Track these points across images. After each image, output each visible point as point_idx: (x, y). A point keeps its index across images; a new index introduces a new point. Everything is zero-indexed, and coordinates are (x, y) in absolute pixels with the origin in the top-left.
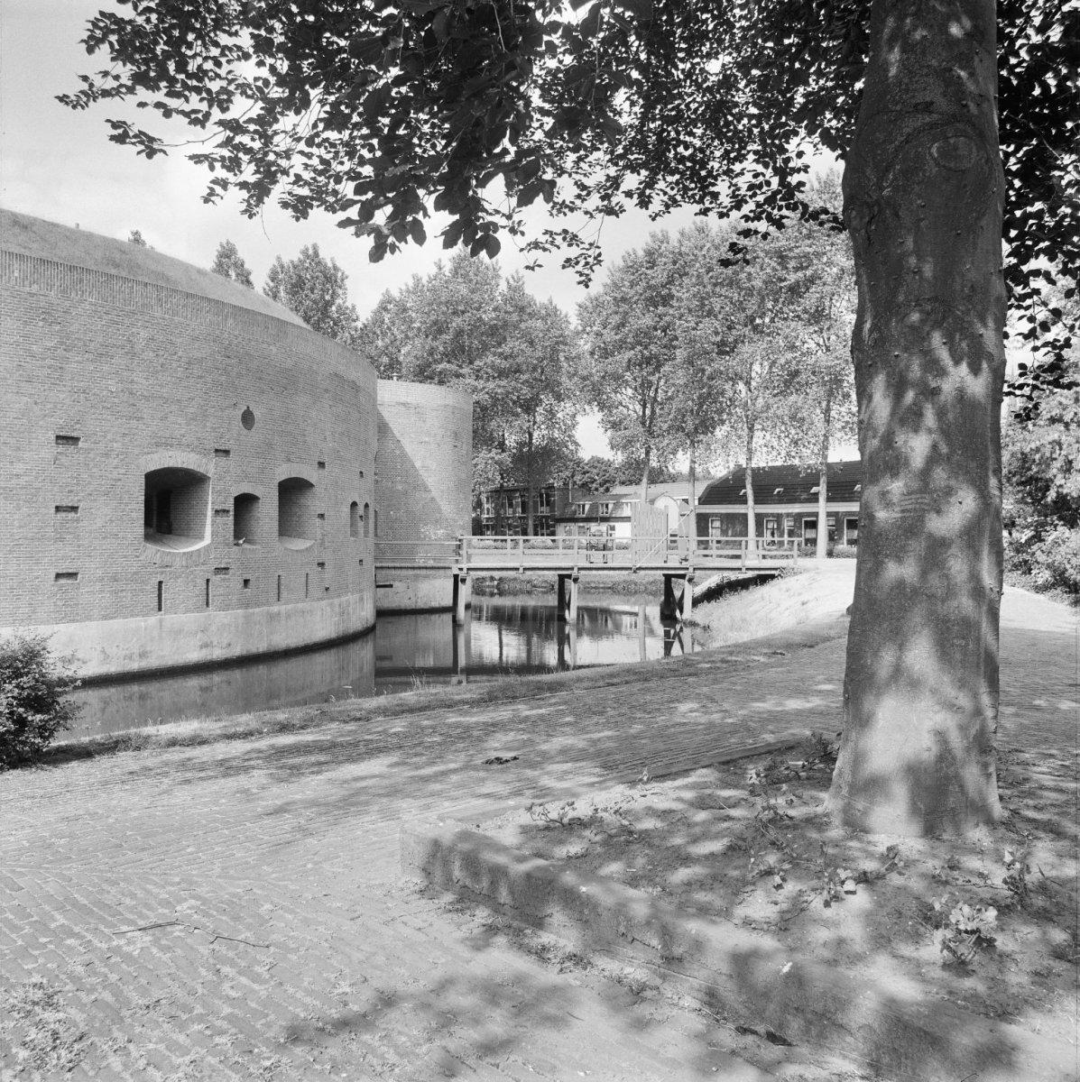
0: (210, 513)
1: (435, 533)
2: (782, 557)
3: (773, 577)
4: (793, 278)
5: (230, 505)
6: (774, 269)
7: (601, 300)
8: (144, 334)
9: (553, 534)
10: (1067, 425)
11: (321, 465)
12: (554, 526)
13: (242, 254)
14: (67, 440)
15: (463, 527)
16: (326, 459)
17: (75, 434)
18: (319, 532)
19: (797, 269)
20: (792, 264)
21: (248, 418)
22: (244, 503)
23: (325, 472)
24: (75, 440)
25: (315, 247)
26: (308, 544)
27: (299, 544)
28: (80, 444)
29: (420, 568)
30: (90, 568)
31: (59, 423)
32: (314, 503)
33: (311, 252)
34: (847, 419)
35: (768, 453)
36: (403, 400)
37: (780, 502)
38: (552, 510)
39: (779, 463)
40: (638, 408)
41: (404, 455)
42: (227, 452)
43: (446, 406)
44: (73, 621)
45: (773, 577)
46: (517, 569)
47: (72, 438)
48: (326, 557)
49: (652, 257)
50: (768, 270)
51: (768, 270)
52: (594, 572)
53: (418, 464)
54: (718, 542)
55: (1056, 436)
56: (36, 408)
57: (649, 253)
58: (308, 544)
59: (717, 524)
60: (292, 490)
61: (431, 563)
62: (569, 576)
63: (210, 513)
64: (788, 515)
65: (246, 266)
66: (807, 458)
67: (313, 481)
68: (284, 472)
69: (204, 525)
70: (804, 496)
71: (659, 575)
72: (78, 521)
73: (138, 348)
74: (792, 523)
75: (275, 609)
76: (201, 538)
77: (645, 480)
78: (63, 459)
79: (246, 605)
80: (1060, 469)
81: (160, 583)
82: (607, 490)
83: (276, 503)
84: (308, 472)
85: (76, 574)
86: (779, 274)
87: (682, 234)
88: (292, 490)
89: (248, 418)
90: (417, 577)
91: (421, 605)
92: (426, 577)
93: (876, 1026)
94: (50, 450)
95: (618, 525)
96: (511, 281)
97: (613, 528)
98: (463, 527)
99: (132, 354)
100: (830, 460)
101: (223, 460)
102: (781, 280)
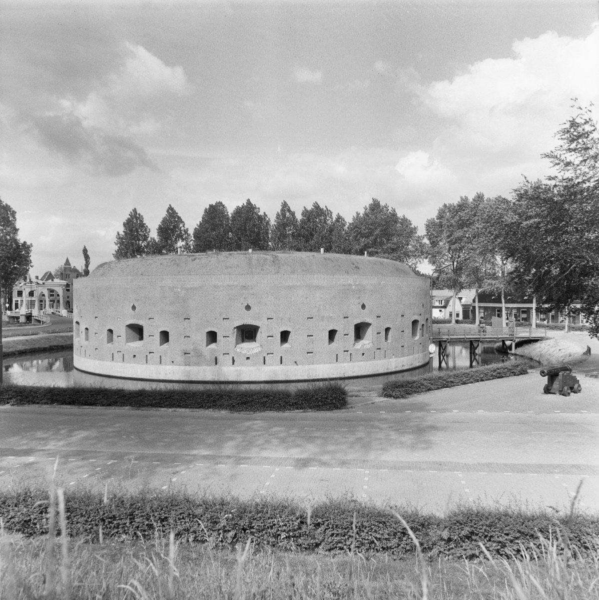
3: (539, 340)
30: (406, 346)
45: (539, 340)
63: (419, 329)
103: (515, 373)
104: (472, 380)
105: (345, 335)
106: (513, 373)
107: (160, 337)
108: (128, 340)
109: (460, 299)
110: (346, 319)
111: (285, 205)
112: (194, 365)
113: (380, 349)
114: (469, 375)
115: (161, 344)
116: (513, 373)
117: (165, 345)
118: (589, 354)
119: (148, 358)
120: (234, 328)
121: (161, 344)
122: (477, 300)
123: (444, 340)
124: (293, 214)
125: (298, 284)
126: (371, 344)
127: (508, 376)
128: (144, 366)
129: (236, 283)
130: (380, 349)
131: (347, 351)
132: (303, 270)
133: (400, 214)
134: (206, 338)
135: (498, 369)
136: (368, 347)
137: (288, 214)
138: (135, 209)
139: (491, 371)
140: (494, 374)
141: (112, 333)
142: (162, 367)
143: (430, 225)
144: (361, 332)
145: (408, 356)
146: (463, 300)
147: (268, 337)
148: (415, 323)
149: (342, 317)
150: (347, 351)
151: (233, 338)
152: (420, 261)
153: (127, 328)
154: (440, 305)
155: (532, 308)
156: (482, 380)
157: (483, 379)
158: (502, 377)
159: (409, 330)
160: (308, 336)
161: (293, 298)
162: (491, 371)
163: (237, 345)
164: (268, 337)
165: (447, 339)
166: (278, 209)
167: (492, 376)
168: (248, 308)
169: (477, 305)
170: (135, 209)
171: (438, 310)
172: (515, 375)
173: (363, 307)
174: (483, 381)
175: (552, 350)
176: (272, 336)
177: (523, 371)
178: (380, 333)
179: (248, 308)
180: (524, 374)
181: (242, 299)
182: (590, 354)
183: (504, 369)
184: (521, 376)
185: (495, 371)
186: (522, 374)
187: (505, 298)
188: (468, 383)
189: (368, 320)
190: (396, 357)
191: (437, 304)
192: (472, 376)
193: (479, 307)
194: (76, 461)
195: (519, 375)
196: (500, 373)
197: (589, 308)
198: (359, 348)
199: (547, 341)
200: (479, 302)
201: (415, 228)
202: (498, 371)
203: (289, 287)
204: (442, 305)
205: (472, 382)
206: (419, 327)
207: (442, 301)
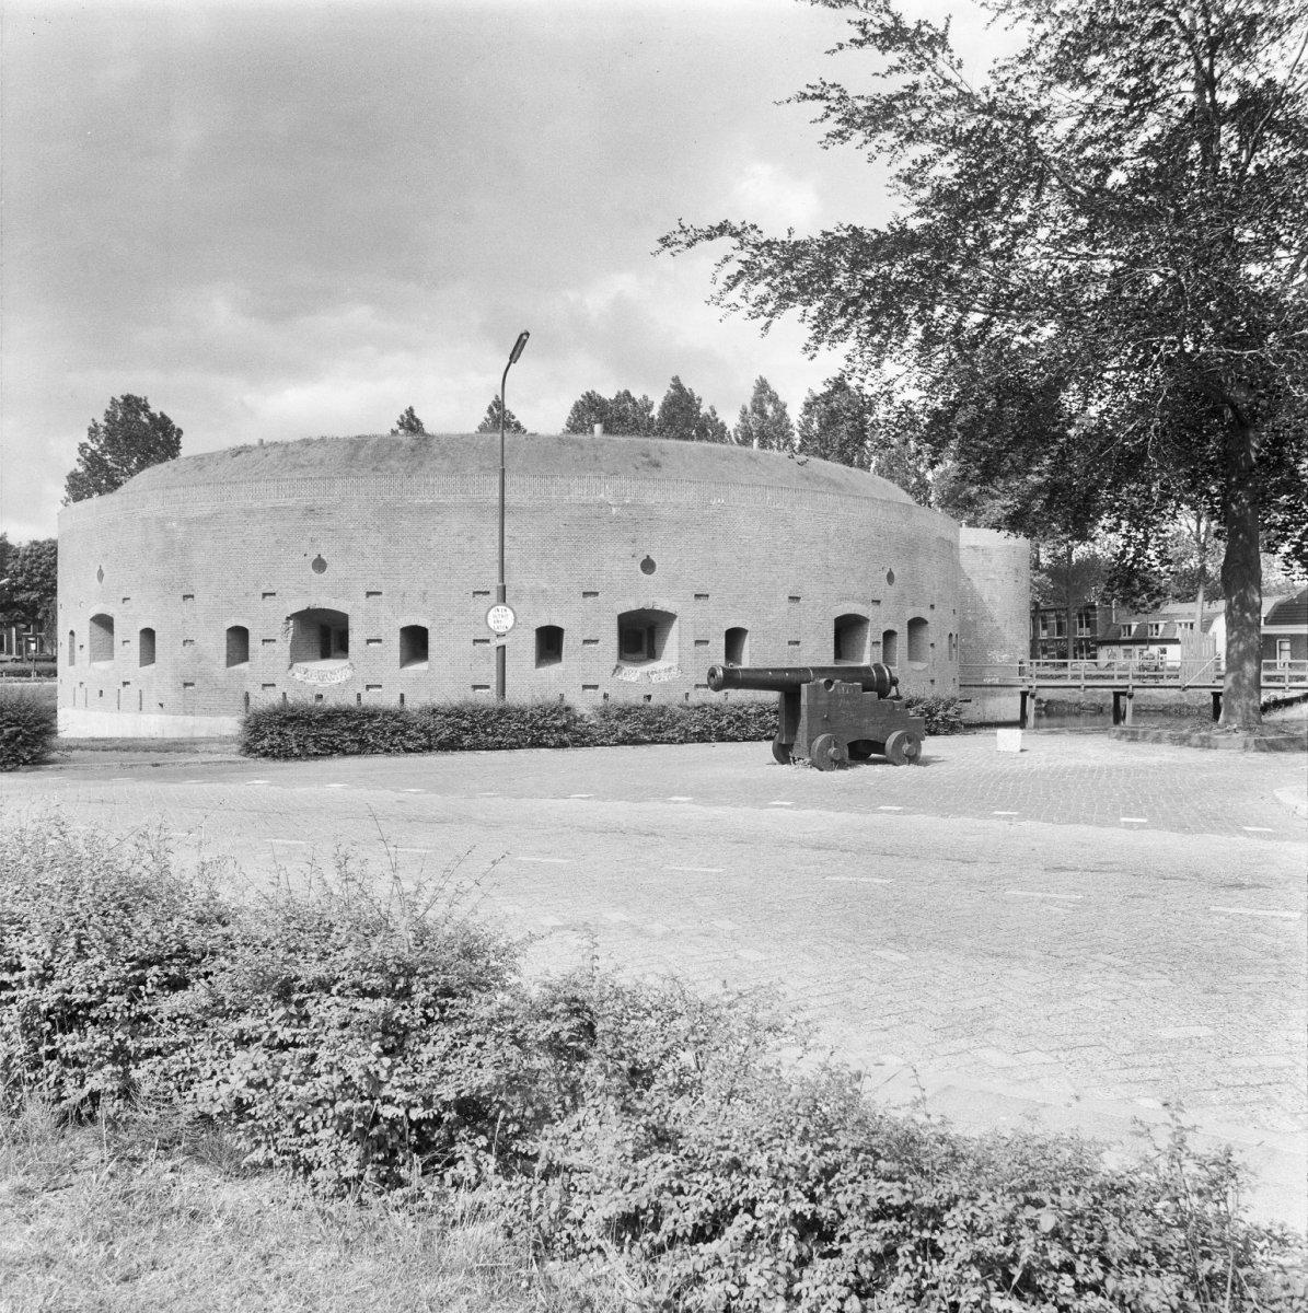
1: (999, 657)
5: (881, 639)
8: (833, 527)
9: (1094, 657)
11: (932, 607)
12: (1095, 649)
13: (775, 386)
15: (1023, 652)
16: (935, 602)
18: (931, 656)
21: (890, 577)
23: (934, 612)
24: (798, 599)
26: (925, 665)
27: (919, 666)
29: (986, 686)
31: (790, 589)
32: (929, 635)
36: (972, 543)
38: (1093, 631)
41: (973, 590)
42: (878, 602)
48: (935, 676)
53: (985, 598)
54: (1290, 664)
58: (925, 665)
59: (1287, 646)
60: (916, 624)
61: (997, 682)
62: (1124, 694)
63: (868, 642)
65: (780, 399)
67: (927, 619)
68: (910, 614)
71: (1207, 692)
73: (831, 537)
77: (1200, 597)
82: (1157, 606)
84: (926, 614)
88: (916, 624)
89: (890, 577)
90: (985, 694)
91: (988, 719)
92: (993, 695)
94: (786, 605)
95: (1169, 647)
97: (1164, 651)
98: (1023, 652)
101: (876, 608)
105: (585, 642)
107: (228, 641)
108: (297, 656)
110: (590, 599)
111: (763, 386)
112: (201, 714)
115: (405, 662)
117: (419, 667)
119: (122, 697)
120: (288, 618)
121: (405, 662)
124: (781, 410)
125: (450, 499)
126: (675, 673)
128: (115, 715)
129: (291, 502)
131: (596, 687)
132: (482, 468)
134: (225, 645)
136: (665, 678)
137: (770, 409)
138: (411, 409)
141: (112, 632)
142: (144, 717)
144: (656, 646)
147: (369, 641)
149: (578, 591)
150: (596, 687)
151: (283, 647)
153: (95, 625)
160: (475, 641)
161: (435, 538)
163: (297, 665)
164: (369, 641)
166: (747, 396)
168: (320, 565)
170: (411, 409)
173: (648, 566)
176: (379, 641)
178: (707, 642)
179: (320, 565)
181: (306, 543)
189: (663, 604)
194: (791, 807)
198: (634, 679)
203: (424, 510)
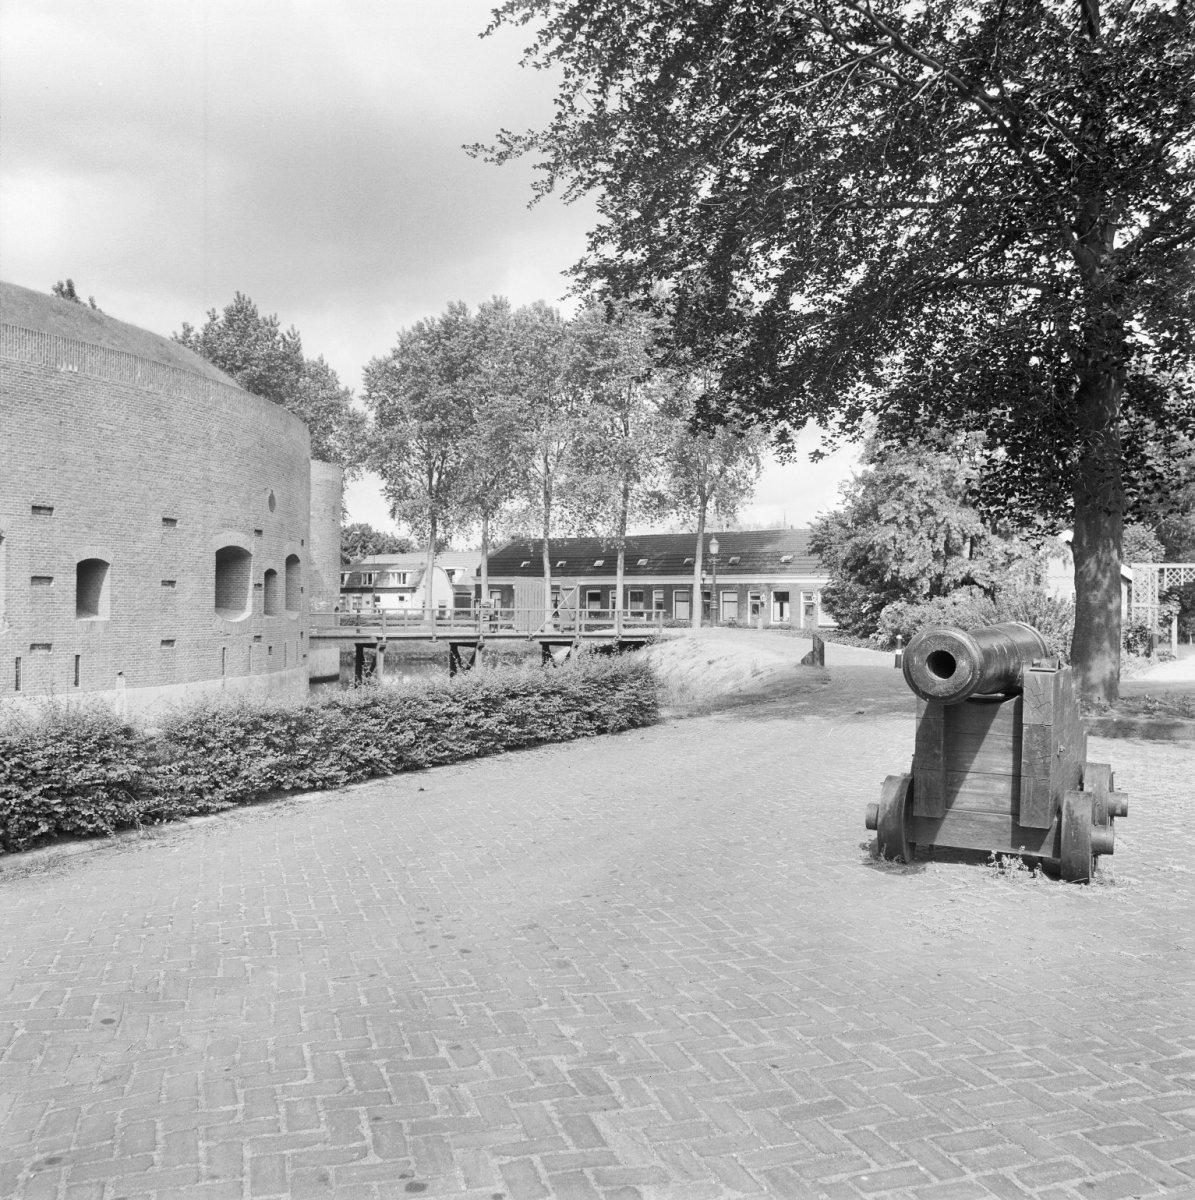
0: (251, 586)
2: (642, 626)
3: (642, 643)
4: (601, 364)
6: (584, 355)
7: (390, 365)
8: (216, 428)
10: (899, 525)
14: (169, 521)
17: (174, 517)
19: (604, 357)
20: (601, 351)
22: (270, 574)
25: (70, 284)
28: (178, 526)
30: (183, 637)
33: (65, 287)
34: (644, 499)
35: (563, 526)
37: (646, 573)
39: (574, 535)
40: (425, 478)
43: (327, 481)
44: (172, 683)
45: (642, 643)
46: (431, 638)
47: (45, 508)
49: (449, 328)
50: (578, 355)
51: (578, 355)
52: (496, 640)
55: (892, 534)
56: (150, 493)
57: (447, 324)
63: (251, 586)
64: (658, 587)
66: (603, 529)
69: (245, 597)
70: (589, 569)
72: (176, 593)
74: (662, 596)
75: (284, 673)
76: (242, 608)
78: (167, 540)
79: (271, 670)
80: (895, 559)
81: (78, 657)
83: (213, 581)
85: (172, 641)
86: (588, 359)
87: (483, 310)
88: (292, 561)
93: (1106, 644)
95: (383, 596)
96: (288, 338)
97: (377, 599)
99: (209, 446)
100: (628, 534)
102: (589, 365)
103: (603, 718)
104: (322, 770)
106: (591, 717)
109: (451, 573)
113: (48, 646)
114: (303, 728)
116: (591, 717)
118: (818, 664)
122: (484, 572)
123: (368, 641)
127: (569, 738)
130: (48, 646)
133: (309, 354)
135: (514, 696)
139: (471, 707)
140: (489, 723)
143: (379, 376)
145: (193, 680)
146: (457, 579)
148: (229, 560)
152: (353, 475)
154: (402, 585)
155: (614, 587)
156: (407, 765)
157: (419, 754)
158: (536, 742)
159: (200, 582)
162: (471, 707)
165: (379, 638)
167: (473, 737)
169: (485, 581)
171: (396, 596)
172: (601, 731)
174: (416, 767)
175: (685, 665)
177: (642, 708)
180: (645, 725)
182: (822, 664)
183: (545, 695)
184: (632, 736)
185: (491, 704)
186: (633, 724)
187: (553, 562)
188: (297, 790)
190: (129, 684)
191: (393, 582)
192: (330, 741)
193: (490, 587)
195: (622, 729)
196: (520, 720)
197: (1066, 286)
199: (664, 644)
200: (490, 573)
201: (347, 393)
202: (513, 704)
204: (406, 586)
205: (328, 784)
206: (254, 574)
207: (404, 575)
